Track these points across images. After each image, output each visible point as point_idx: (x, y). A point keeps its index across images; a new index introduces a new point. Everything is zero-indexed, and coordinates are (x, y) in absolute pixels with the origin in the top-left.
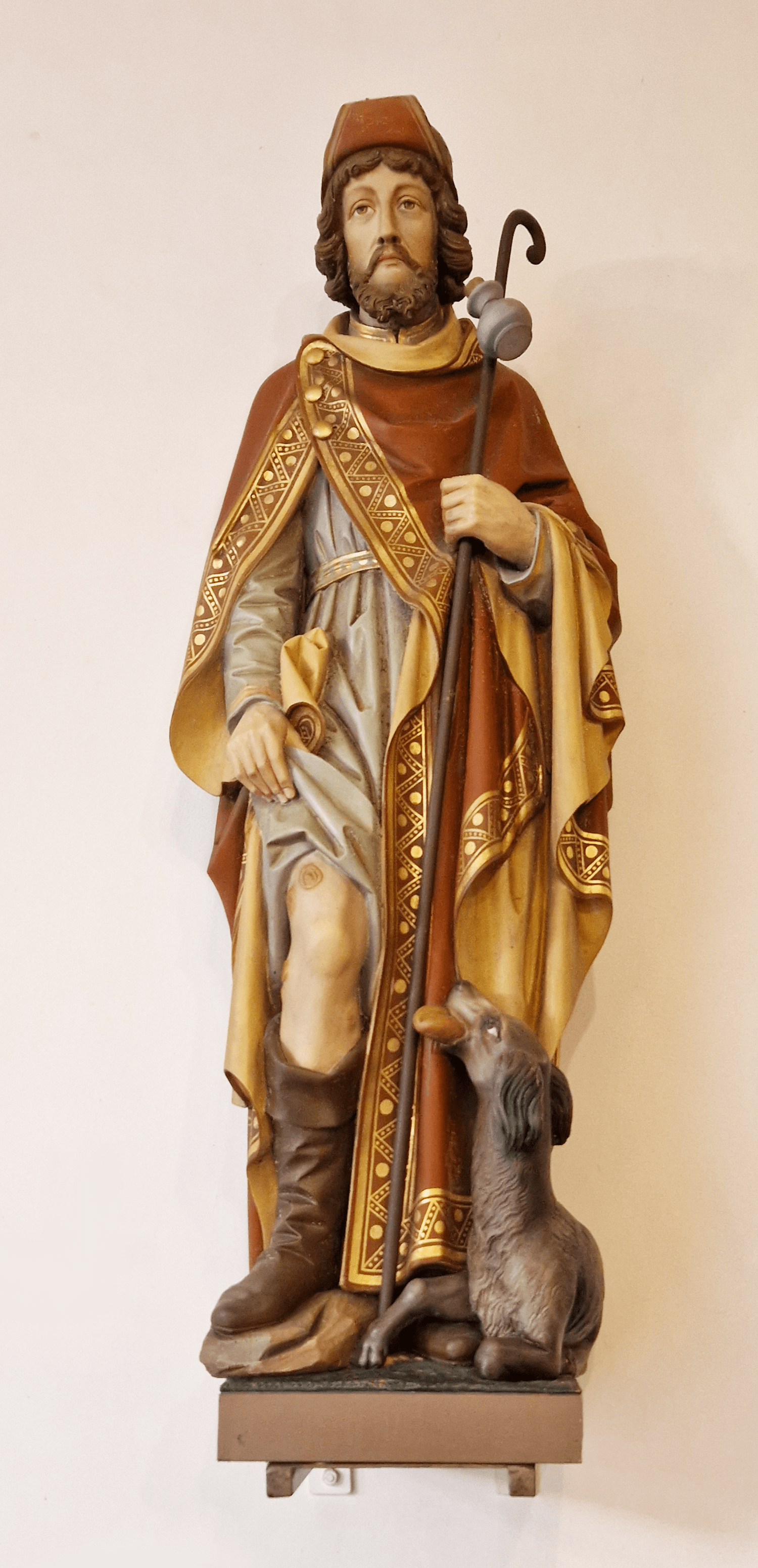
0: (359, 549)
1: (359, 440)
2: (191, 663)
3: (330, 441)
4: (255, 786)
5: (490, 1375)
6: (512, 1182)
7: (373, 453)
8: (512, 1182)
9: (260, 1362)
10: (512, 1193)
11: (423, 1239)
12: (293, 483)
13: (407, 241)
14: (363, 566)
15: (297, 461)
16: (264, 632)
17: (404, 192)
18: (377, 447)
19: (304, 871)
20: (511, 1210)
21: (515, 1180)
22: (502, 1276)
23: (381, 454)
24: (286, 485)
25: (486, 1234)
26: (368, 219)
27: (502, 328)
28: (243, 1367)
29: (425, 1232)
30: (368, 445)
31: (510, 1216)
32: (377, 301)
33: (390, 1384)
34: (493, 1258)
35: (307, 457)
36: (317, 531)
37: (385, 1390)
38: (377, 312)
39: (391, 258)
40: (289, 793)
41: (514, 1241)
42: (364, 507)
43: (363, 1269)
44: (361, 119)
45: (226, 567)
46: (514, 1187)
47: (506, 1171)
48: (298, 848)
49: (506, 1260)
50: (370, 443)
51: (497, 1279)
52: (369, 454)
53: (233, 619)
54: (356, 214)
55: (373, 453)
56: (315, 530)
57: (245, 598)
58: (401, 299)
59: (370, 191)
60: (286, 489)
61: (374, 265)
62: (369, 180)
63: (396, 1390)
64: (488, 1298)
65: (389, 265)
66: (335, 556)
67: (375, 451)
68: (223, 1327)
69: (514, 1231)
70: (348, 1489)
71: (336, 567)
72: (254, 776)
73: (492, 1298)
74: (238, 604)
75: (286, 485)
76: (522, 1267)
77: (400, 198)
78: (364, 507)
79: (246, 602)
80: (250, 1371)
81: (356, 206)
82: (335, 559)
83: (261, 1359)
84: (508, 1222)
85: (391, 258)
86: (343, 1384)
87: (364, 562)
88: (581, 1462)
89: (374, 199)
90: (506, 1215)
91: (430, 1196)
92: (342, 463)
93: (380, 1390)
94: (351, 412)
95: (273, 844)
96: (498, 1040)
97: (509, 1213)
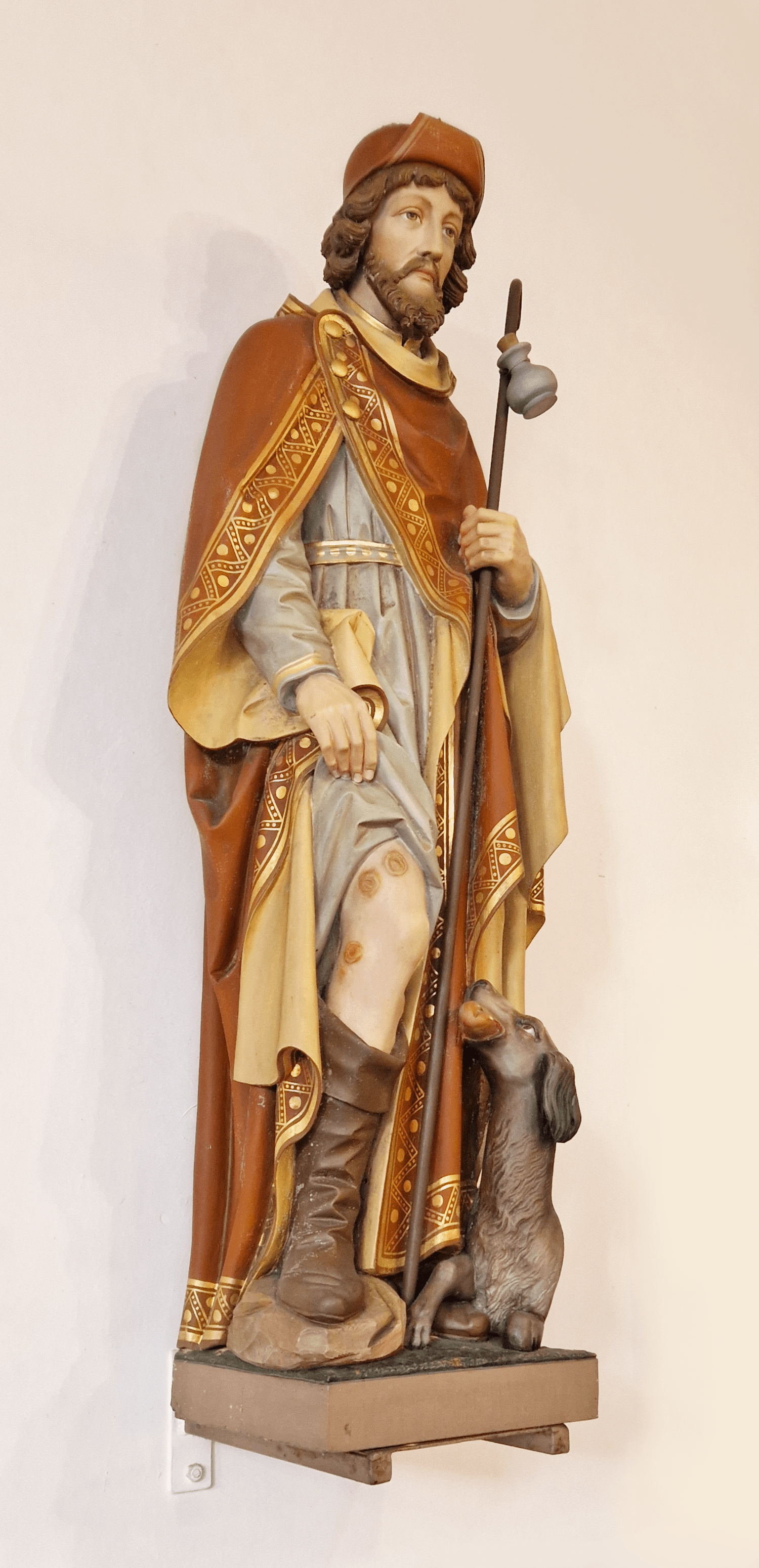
0: (375, 540)
1: (382, 432)
2: (215, 604)
3: (357, 424)
4: (337, 760)
5: (526, 1347)
6: (543, 1169)
7: (394, 451)
8: (543, 1169)
9: (370, 1349)
10: (541, 1179)
11: (448, 1222)
12: (320, 450)
13: (441, 264)
14: (382, 559)
15: (323, 430)
16: (306, 598)
17: (450, 220)
18: (398, 447)
19: (388, 856)
20: (538, 1195)
21: (545, 1167)
22: (526, 1257)
23: (401, 454)
24: (312, 450)
25: (514, 1219)
26: (415, 227)
27: (543, 392)
28: (352, 1355)
29: (449, 1215)
30: (389, 441)
31: (537, 1201)
32: (411, 307)
33: (462, 1361)
34: (518, 1240)
35: (332, 429)
36: (330, 506)
37: (462, 1367)
38: (405, 316)
39: (428, 273)
40: (369, 775)
41: (539, 1223)
42: (392, 503)
43: (385, 1253)
44: (437, 135)
45: (254, 514)
46: (542, 1175)
47: (538, 1160)
48: (386, 833)
49: (532, 1240)
50: (392, 441)
51: (522, 1258)
52: (391, 450)
53: (268, 572)
54: (405, 216)
55: (394, 451)
56: (327, 505)
57: (282, 555)
58: (429, 315)
59: (428, 205)
60: (313, 454)
61: (411, 269)
62: (429, 194)
63: (470, 1367)
64: (505, 1276)
65: (425, 279)
66: (346, 536)
67: (395, 450)
68: (335, 1315)
69: (539, 1214)
70: (209, 1483)
71: (348, 549)
72: (344, 751)
73: (509, 1276)
74: (276, 558)
75: (312, 450)
76: (546, 1247)
77: (448, 223)
78: (392, 503)
79: (282, 559)
80: (358, 1358)
81: (408, 210)
82: (345, 539)
83: (369, 1346)
84: (536, 1205)
85: (428, 273)
86: (429, 1365)
87: (383, 555)
88: (597, 1417)
89: (426, 212)
90: (534, 1200)
91: (448, 1181)
92: (370, 451)
93: (455, 1368)
94: (379, 403)
95: (363, 824)
96: (537, 1040)
97: (537, 1198)
